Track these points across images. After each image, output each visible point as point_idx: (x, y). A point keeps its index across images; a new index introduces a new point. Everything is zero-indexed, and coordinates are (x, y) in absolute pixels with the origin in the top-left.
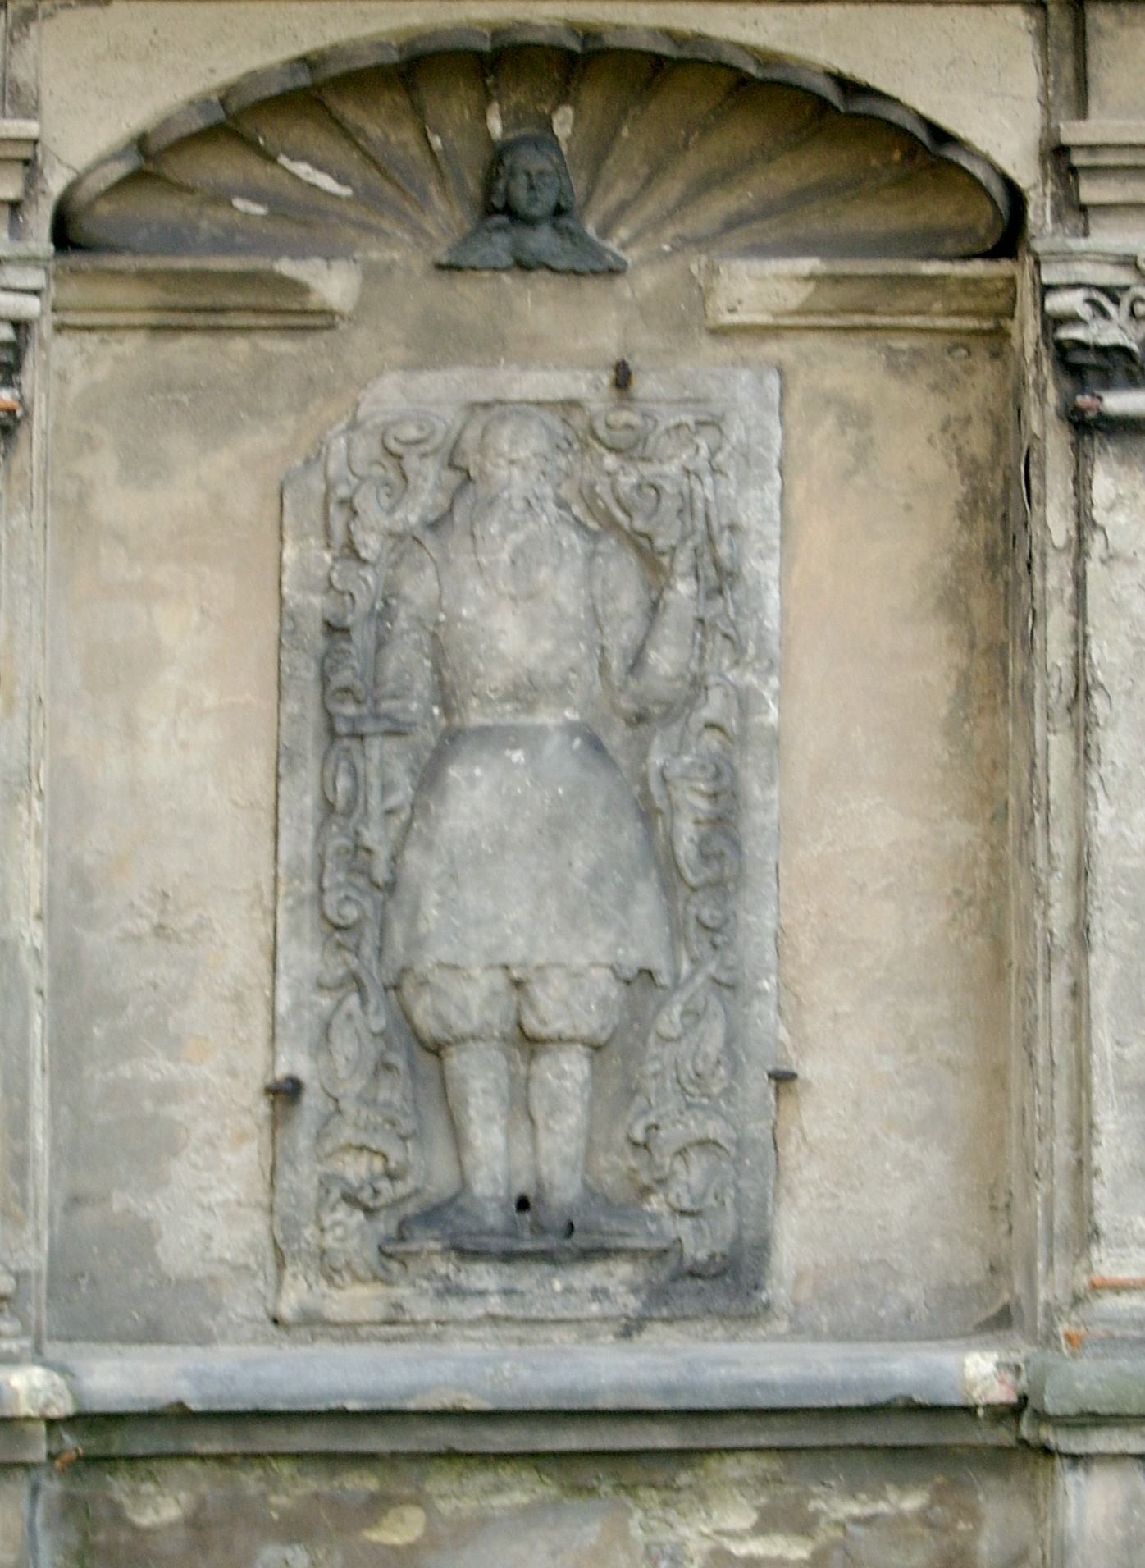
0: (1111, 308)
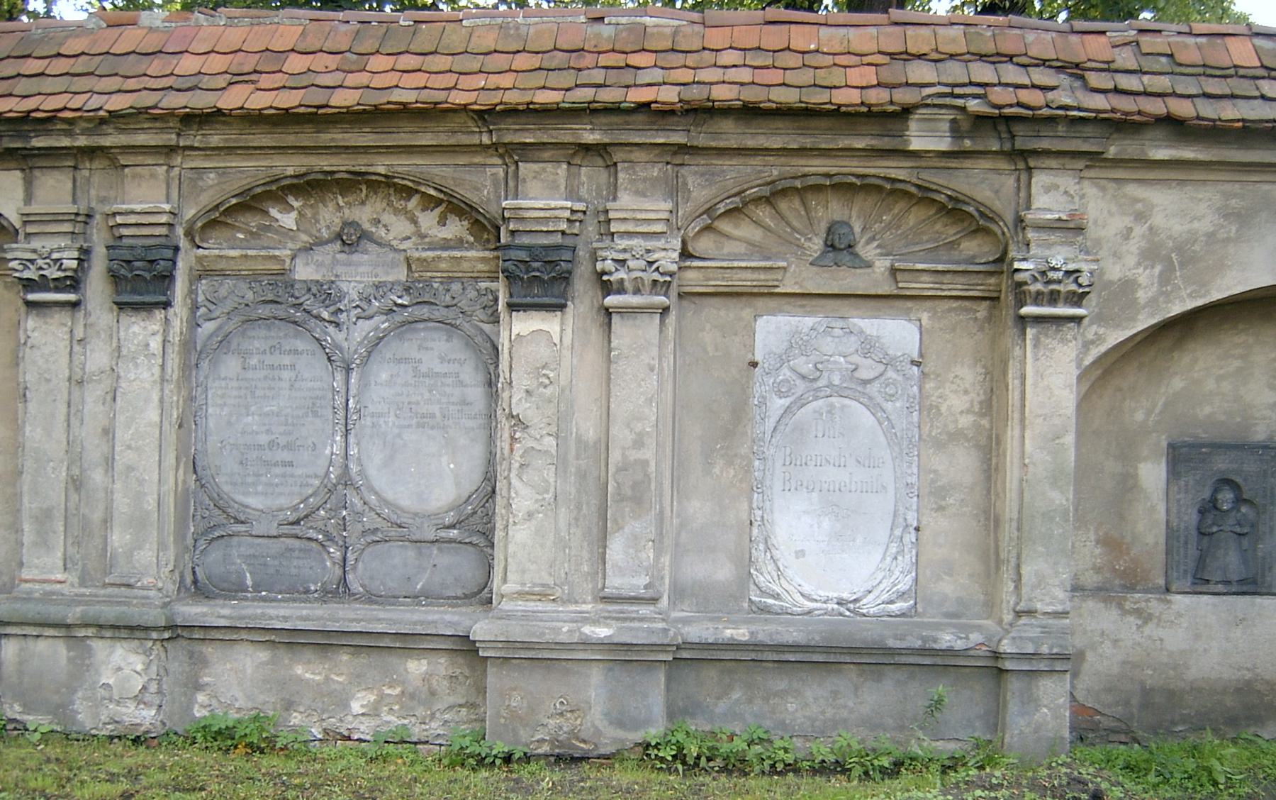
0: (31, 267)
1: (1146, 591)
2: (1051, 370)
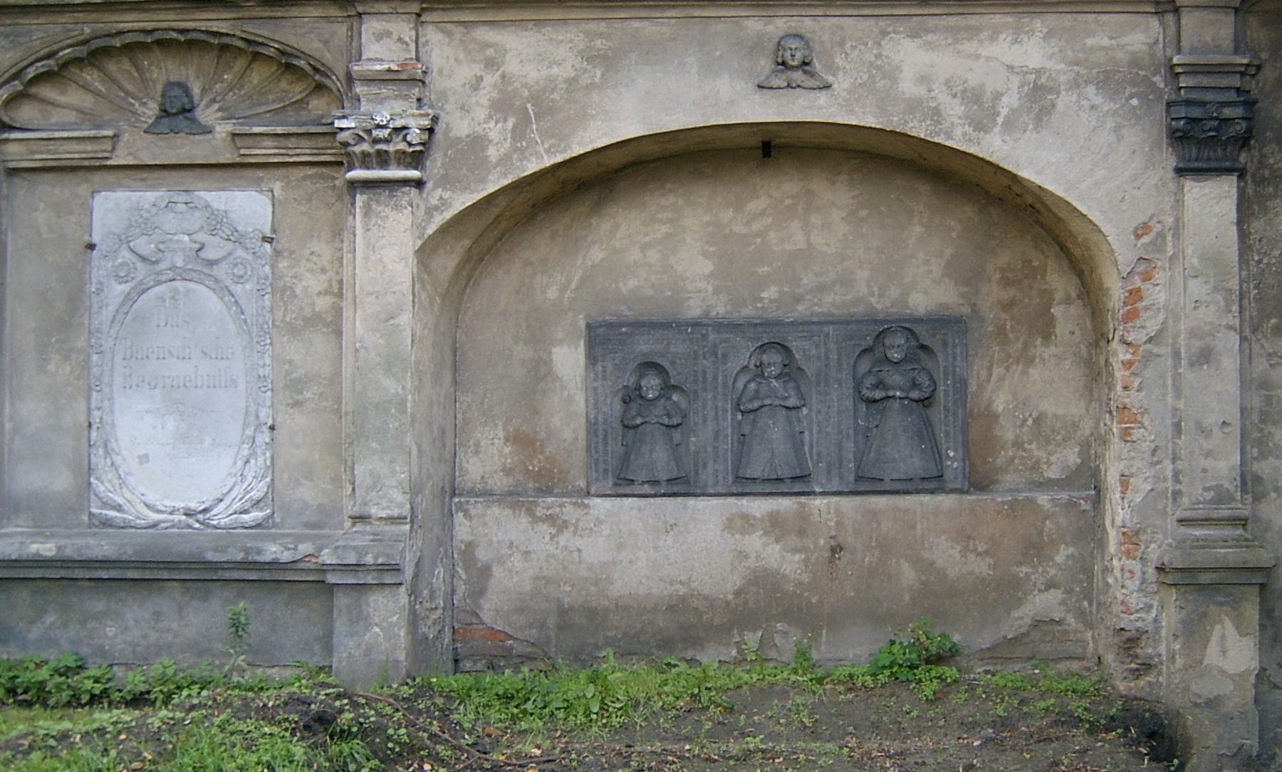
1: (563, 495)
2: (384, 241)
